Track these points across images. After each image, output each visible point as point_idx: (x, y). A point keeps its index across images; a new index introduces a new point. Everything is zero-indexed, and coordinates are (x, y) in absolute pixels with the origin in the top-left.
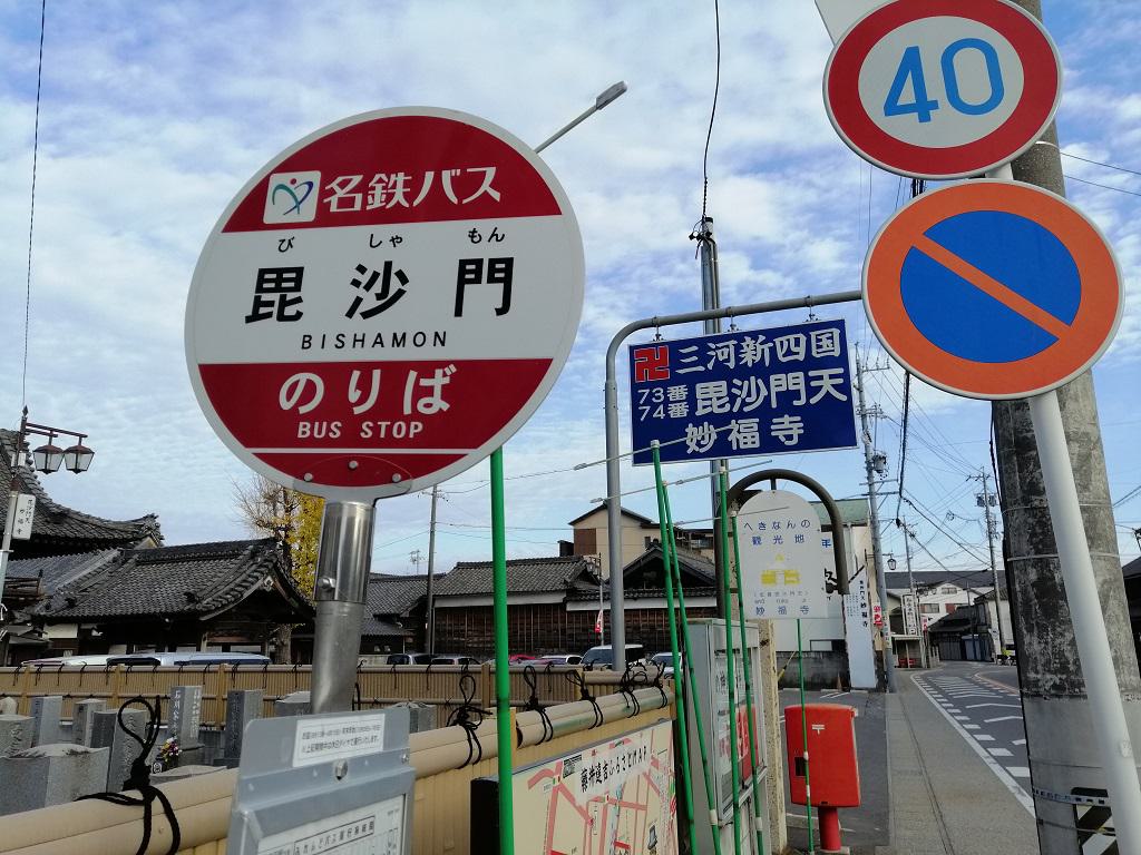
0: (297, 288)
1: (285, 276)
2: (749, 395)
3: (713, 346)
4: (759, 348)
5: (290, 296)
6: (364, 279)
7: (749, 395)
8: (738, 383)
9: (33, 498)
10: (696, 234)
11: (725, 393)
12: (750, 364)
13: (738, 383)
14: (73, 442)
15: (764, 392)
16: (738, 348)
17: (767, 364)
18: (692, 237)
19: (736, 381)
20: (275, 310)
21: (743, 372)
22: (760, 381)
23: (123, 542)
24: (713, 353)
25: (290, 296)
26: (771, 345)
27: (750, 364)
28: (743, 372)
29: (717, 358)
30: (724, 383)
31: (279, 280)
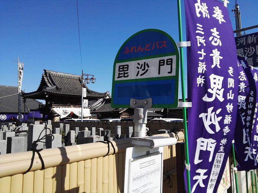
0: (127, 70)
1: (125, 67)
2: (250, 51)
3: (239, 39)
4: (253, 38)
5: (126, 72)
6: (139, 66)
7: (250, 51)
8: (247, 49)
9: (86, 89)
10: (233, 10)
11: (243, 52)
12: (250, 43)
13: (247, 49)
14: (92, 77)
15: (254, 50)
16: (246, 39)
17: (255, 42)
18: (232, 11)
19: (246, 48)
20: (123, 75)
21: (248, 45)
22: (253, 48)
23: (103, 97)
24: (239, 41)
25: (126, 72)
26: (256, 37)
27: (250, 43)
28: (248, 45)
29: (240, 42)
30: (242, 49)
31: (123, 68)
